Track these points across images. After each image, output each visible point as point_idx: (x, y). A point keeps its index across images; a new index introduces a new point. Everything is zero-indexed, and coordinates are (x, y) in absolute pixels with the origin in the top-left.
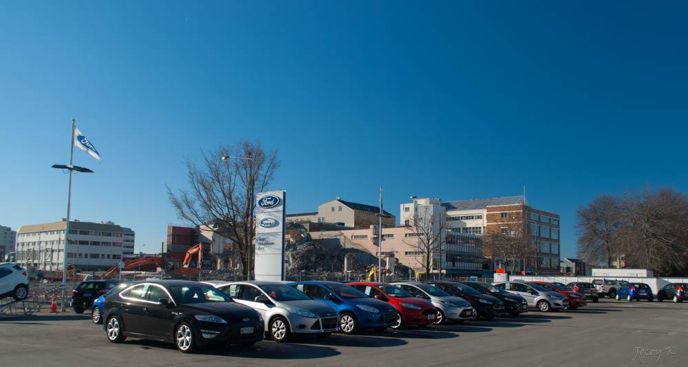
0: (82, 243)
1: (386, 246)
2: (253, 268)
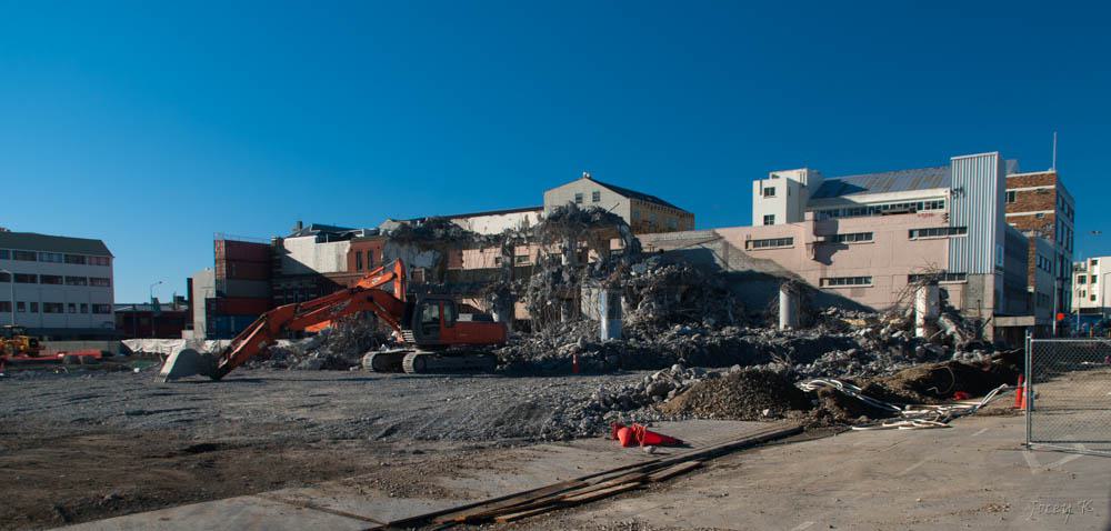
0: (20, 278)
1: (845, 262)
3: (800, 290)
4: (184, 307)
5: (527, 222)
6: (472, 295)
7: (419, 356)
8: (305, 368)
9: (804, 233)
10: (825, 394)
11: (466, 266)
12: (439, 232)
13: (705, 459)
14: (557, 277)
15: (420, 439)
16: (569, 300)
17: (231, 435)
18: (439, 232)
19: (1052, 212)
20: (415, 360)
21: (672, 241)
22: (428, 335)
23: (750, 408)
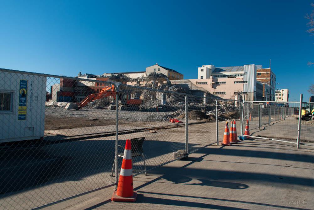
1: (219, 88)
2: (282, 103)
3: (209, 95)
5: (143, 76)
7: (122, 107)
12: (121, 77)
18: (121, 77)
19: (270, 78)
21: (178, 82)
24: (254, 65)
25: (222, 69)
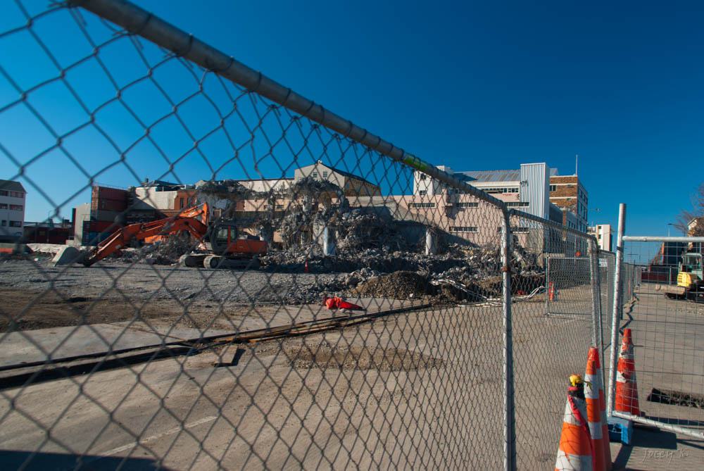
1: (462, 218)
3: (439, 234)
4: (70, 226)
5: (284, 186)
6: (249, 226)
7: (214, 258)
8: (143, 263)
9: (441, 201)
10: (444, 287)
11: (246, 209)
12: (231, 189)
13: (372, 318)
14: (299, 218)
15: (211, 300)
16: (306, 232)
17: (95, 294)
18: (231, 189)
19: (576, 197)
20: (211, 261)
21: (364, 200)
22: (219, 245)
23: (403, 292)
24: (544, 163)
25: (469, 175)
